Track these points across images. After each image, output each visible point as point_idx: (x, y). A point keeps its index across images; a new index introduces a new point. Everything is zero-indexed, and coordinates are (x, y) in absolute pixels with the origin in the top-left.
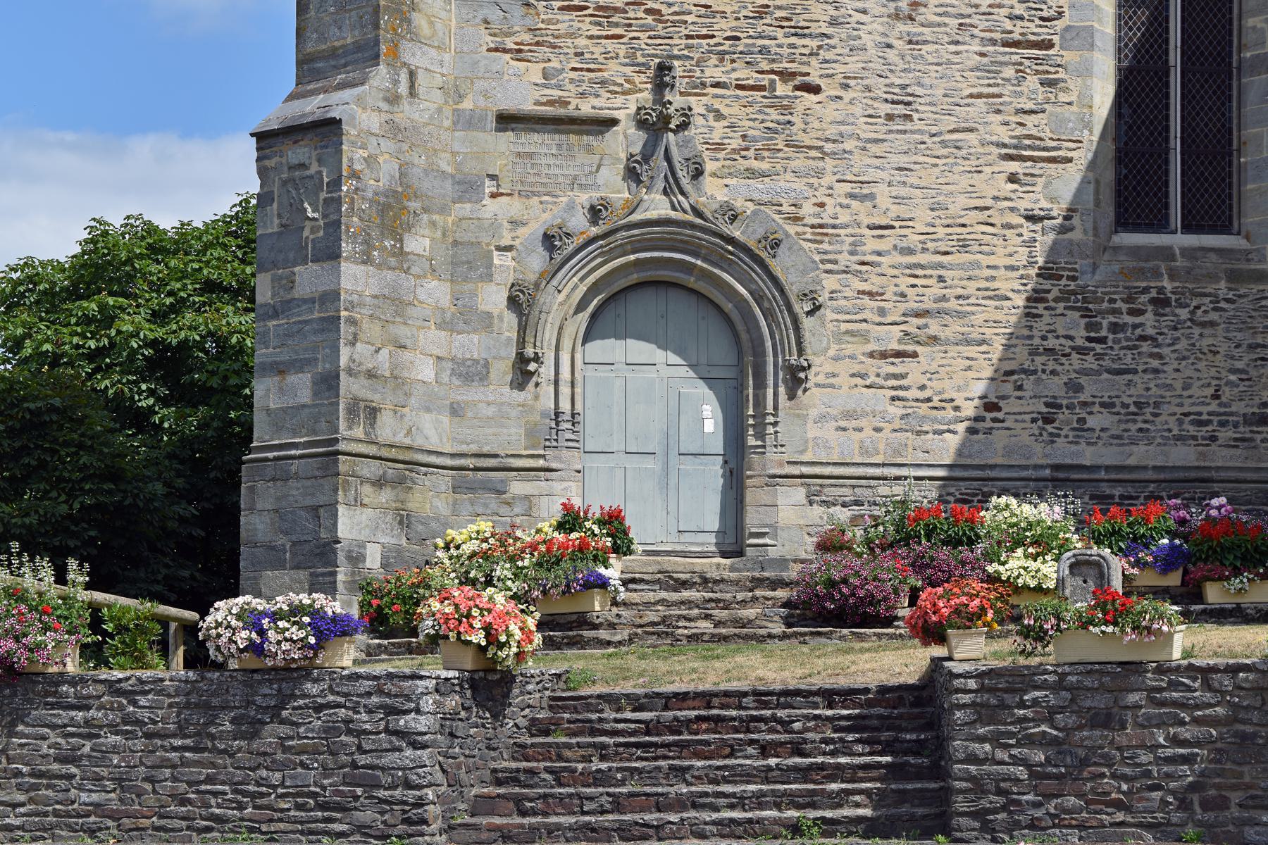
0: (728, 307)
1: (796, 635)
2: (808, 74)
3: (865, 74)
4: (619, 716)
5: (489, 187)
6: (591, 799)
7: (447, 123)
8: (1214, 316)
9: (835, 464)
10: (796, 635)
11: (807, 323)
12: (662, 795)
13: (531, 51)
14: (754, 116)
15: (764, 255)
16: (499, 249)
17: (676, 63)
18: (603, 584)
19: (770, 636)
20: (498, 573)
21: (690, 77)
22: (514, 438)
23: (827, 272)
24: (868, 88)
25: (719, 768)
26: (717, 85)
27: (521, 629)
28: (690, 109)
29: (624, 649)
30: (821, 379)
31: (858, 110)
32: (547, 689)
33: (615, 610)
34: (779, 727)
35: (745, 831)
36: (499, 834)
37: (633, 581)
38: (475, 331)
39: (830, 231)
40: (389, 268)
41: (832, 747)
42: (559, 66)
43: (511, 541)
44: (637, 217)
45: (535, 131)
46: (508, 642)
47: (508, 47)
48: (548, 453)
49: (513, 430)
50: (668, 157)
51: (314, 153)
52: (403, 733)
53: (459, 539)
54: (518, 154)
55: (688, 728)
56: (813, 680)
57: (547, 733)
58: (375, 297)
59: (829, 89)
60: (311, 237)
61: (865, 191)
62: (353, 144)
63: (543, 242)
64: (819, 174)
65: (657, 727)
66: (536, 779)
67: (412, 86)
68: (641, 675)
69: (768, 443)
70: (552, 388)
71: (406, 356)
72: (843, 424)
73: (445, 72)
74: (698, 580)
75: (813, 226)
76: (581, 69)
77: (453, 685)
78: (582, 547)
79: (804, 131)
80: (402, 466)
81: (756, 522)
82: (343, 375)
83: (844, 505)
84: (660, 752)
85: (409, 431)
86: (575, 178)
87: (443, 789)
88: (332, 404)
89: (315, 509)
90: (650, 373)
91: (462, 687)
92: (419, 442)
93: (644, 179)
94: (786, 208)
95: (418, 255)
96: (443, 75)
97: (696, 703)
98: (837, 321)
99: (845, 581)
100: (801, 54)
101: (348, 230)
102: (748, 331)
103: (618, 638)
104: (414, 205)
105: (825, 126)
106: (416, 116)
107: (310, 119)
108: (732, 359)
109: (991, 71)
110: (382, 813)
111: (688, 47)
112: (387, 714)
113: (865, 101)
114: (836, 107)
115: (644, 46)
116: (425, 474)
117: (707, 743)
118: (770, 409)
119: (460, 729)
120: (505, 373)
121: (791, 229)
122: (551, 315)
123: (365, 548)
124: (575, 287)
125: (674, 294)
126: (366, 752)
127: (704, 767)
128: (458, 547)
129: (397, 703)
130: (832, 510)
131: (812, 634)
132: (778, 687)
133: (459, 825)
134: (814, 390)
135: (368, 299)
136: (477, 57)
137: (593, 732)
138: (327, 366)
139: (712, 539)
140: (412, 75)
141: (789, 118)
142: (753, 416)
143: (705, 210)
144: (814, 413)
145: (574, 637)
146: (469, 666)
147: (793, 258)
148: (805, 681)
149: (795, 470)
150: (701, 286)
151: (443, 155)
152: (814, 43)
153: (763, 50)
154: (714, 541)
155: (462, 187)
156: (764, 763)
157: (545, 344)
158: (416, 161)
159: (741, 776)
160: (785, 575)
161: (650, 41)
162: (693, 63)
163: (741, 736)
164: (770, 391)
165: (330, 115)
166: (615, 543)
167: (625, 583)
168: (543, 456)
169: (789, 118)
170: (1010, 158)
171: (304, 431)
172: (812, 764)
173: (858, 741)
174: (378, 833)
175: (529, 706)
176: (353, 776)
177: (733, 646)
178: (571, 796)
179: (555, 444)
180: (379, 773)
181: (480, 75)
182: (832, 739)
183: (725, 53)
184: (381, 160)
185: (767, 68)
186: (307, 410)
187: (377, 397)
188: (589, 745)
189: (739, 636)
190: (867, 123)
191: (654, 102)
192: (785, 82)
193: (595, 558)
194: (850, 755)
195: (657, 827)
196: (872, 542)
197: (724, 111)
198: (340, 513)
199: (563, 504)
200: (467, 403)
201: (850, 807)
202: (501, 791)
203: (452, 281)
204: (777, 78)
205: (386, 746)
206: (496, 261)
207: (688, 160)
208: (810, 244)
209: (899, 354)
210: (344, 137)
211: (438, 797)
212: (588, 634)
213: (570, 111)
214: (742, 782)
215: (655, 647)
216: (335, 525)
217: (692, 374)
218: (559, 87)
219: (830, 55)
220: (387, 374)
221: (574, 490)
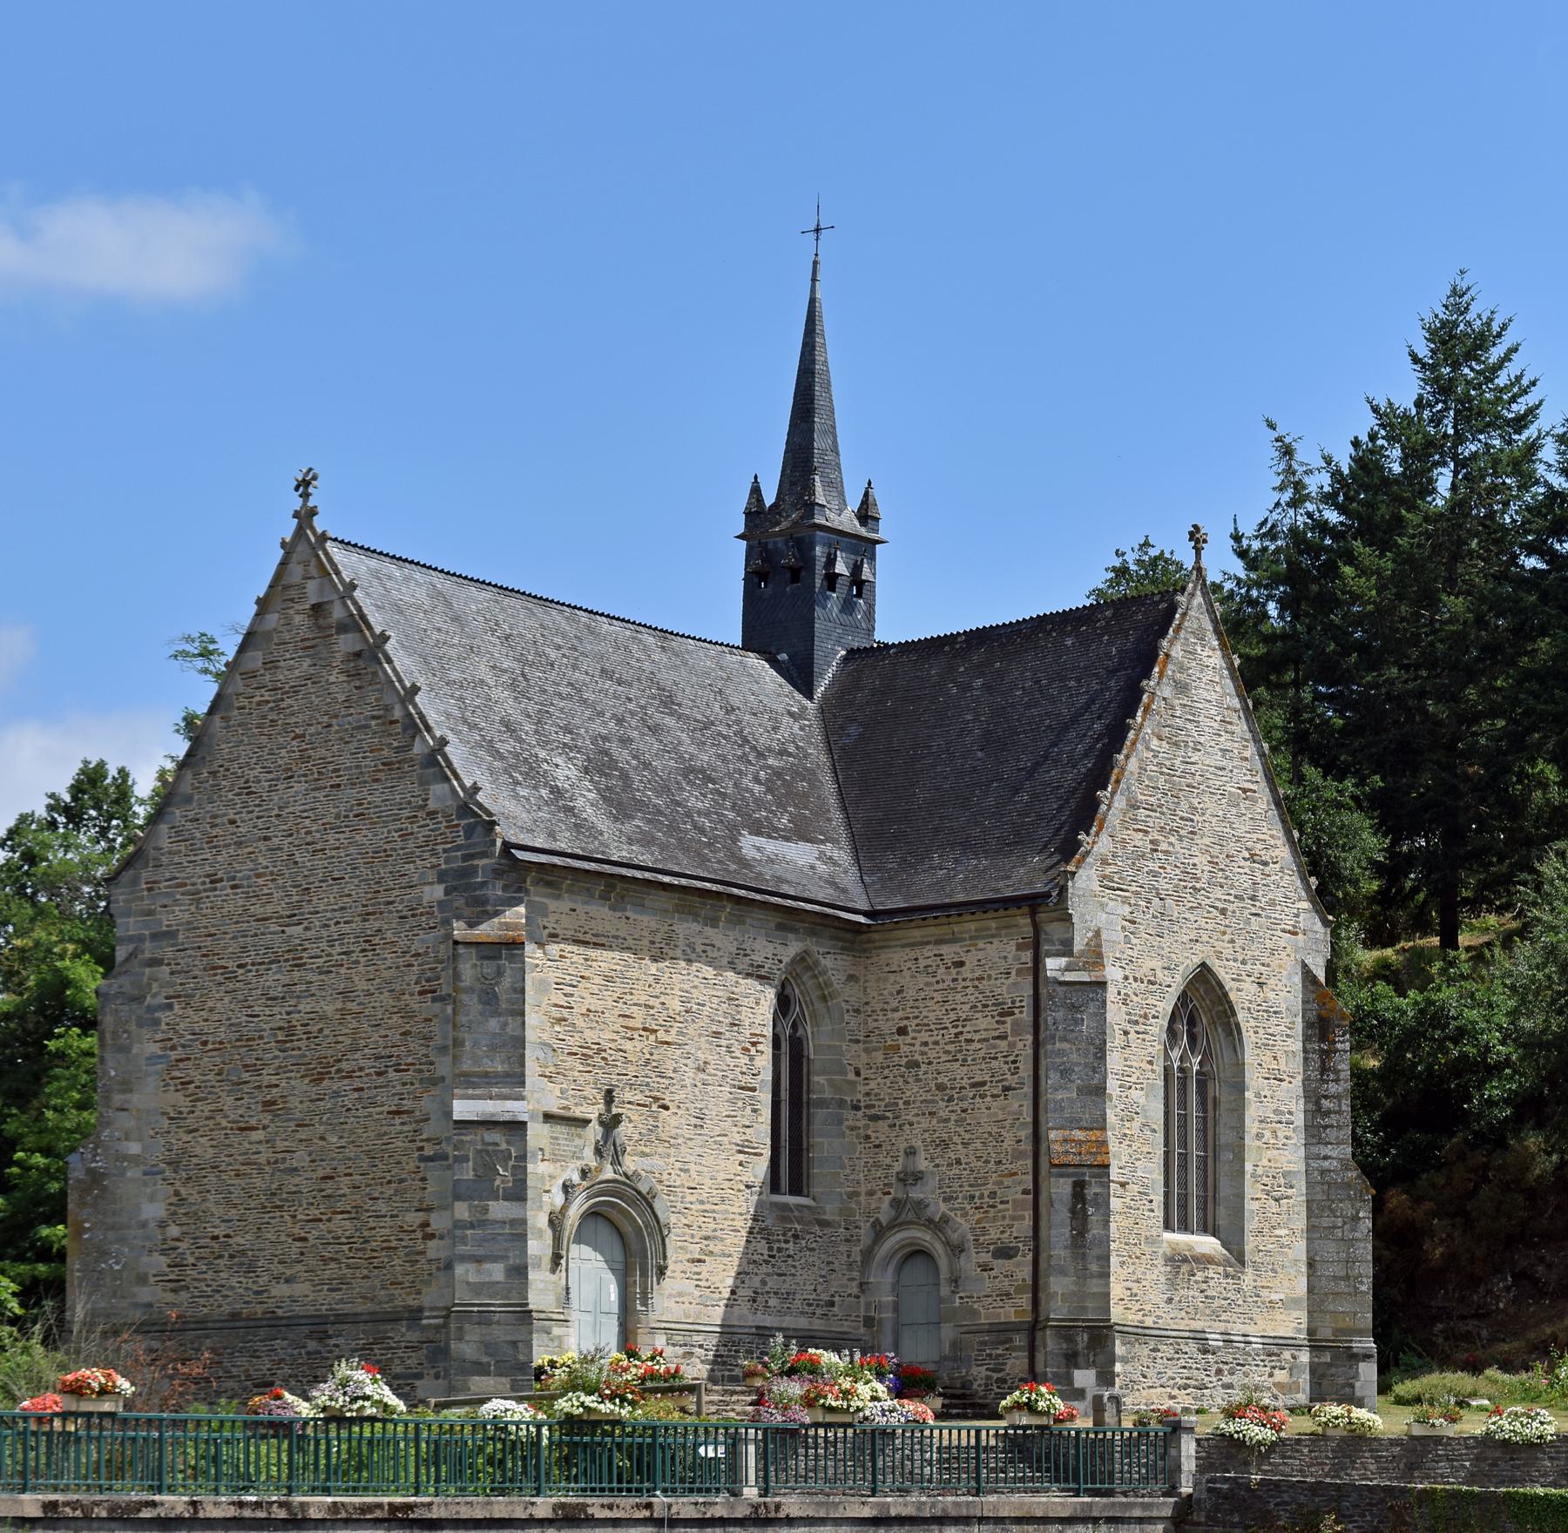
8: (814, 1245)
26: (629, 1103)
59: (673, 1110)
89: (514, 1344)
109: (732, 1102)
121: (659, 1187)
152: (667, 1082)
153: (647, 1085)
170: (740, 1152)
209: (699, 1261)
213: (570, 1114)
218: (567, 1099)
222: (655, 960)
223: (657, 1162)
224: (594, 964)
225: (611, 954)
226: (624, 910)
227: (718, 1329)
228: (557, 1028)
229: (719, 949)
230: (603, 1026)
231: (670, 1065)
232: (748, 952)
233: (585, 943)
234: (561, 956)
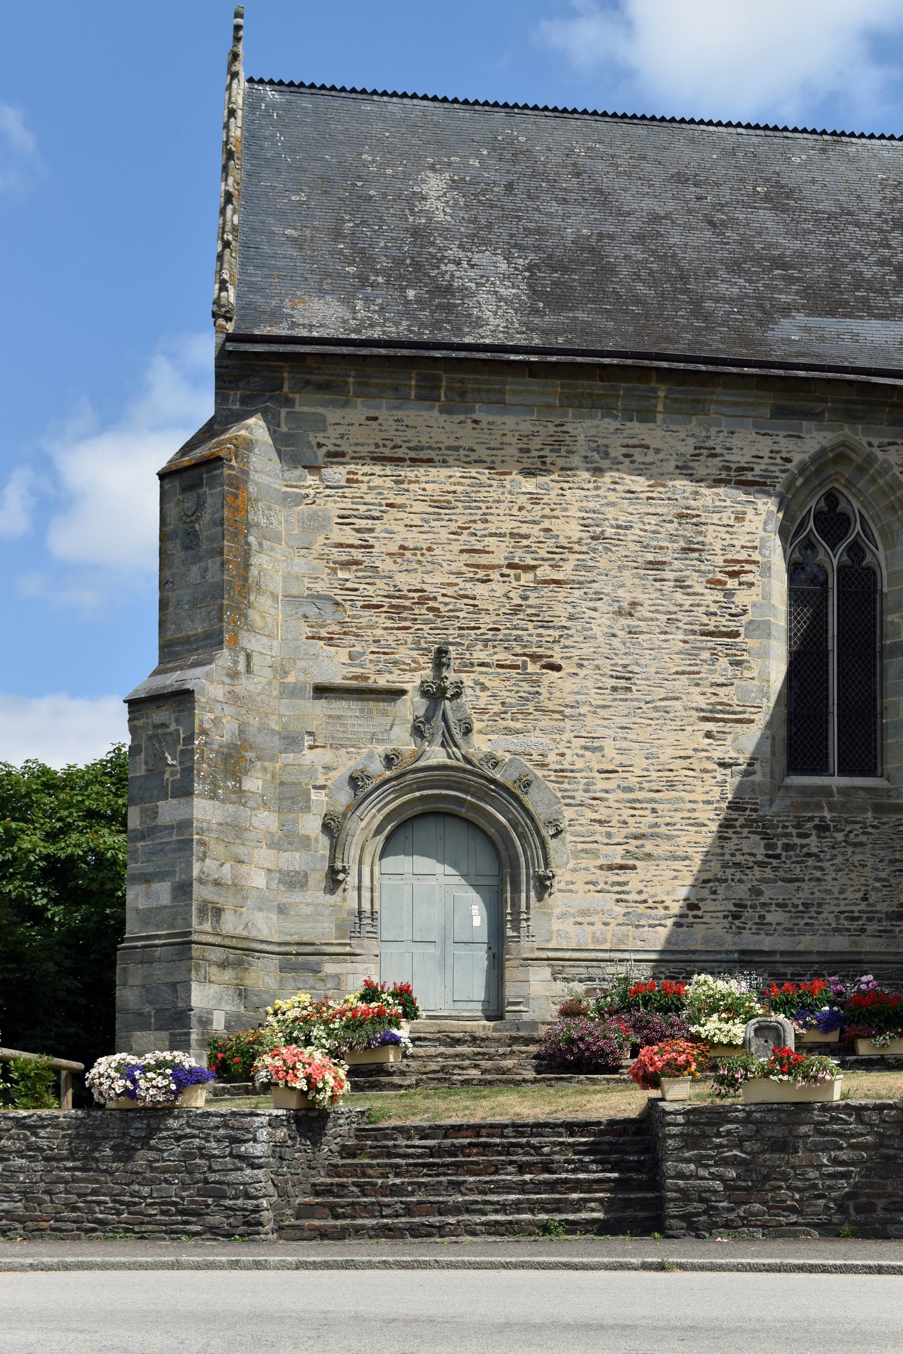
0: (492, 831)
1: (544, 1080)
3: (596, 656)
4: (409, 1143)
5: (308, 741)
6: (388, 1206)
7: (275, 693)
8: (863, 838)
9: (573, 950)
10: (544, 1080)
11: (552, 844)
12: (443, 1202)
15: (518, 792)
16: (315, 787)
17: (451, 648)
18: (396, 1041)
19: (525, 1081)
20: (315, 1033)
23: (566, 805)
24: (598, 667)
25: (486, 1182)
26: (482, 665)
27: (334, 1078)
28: (462, 683)
30: (562, 886)
31: (590, 683)
33: (405, 1061)
34: (532, 1151)
35: (507, 1230)
37: (419, 1039)
38: (297, 850)
39: (570, 774)
40: (231, 803)
42: (361, 650)
44: (421, 763)
45: (343, 699)
46: (324, 1088)
48: (353, 941)
49: (326, 925)
50: (445, 719)
51: (173, 716)
54: (330, 717)
55: (462, 1152)
56: (558, 1115)
57: (354, 1156)
58: (220, 824)
61: (596, 745)
62: (203, 708)
64: (561, 731)
66: (346, 1191)
67: (248, 665)
68: (426, 1111)
70: (356, 893)
71: (244, 868)
72: (579, 920)
75: (556, 771)
76: (378, 653)
78: (380, 1014)
79: (549, 699)
82: (195, 883)
83: (580, 981)
84: (441, 1170)
85: (247, 925)
86: (374, 734)
87: (275, 1199)
88: (186, 905)
89: (173, 985)
91: (289, 1122)
92: (254, 934)
93: (427, 735)
94: (535, 757)
97: (469, 1133)
101: (199, 774)
103: (407, 1082)
104: (250, 755)
105: (565, 695)
106: (251, 688)
107: (170, 690)
108: (494, 871)
109: (692, 653)
110: (228, 1217)
111: (460, 636)
112: (231, 1143)
117: (477, 1163)
118: (523, 909)
120: (320, 881)
121: (540, 773)
123: (212, 1014)
124: (374, 816)
126: (215, 1171)
127: (475, 1182)
128: (284, 1014)
129: (239, 1134)
130: (571, 984)
131: (556, 1079)
132: (531, 1120)
134: (557, 894)
137: (390, 1155)
138: (183, 876)
139: (479, 1006)
140: (248, 657)
141: (537, 689)
144: (557, 911)
149: (543, 955)
150: (471, 816)
151: (272, 717)
153: (518, 639)
155: (287, 741)
156: (522, 1178)
158: (252, 721)
160: (535, 1034)
163: (503, 1158)
166: (404, 1010)
167: (413, 1040)
168: (350, 945)
169: (537, 689)
170: (707, 719)
173: (593, 1162)
176: (205, 1189)
177: (496, 1089)
178: (373, 1203)
180: (225, 1187)
183: (488, 640)
184: (224, 721)
185: (520, 652)
186: (167, 910)
187: (221, 900)
188: (386, 1165)
189: (500, 1081)
191: (434, 678)
192: (534, 662)
193: (390, 1022)
199: (365, 981)
200: (290, 904)
203: (279, 812)
205: (230, 1166)
206: (313, 797)
209: (622, 867)
212: (385, 1079)
215: (436, 1089)
216: (189, 996)
217: (463, 882)
218: (362, 666)
219: (568, 642)
220: (229, 882)
221: (373, 969)
222: (529, 473)
223: (536, 740)
224: (413, 487)
225: (444, 472)
226: (473, 411)
227: (654, 956)
228: (341, 575)
229: (657, 451)
230: (429, 567)
231: (562, 611)
232: (718, 450)
233: (397, 461)
234: (348, 481)
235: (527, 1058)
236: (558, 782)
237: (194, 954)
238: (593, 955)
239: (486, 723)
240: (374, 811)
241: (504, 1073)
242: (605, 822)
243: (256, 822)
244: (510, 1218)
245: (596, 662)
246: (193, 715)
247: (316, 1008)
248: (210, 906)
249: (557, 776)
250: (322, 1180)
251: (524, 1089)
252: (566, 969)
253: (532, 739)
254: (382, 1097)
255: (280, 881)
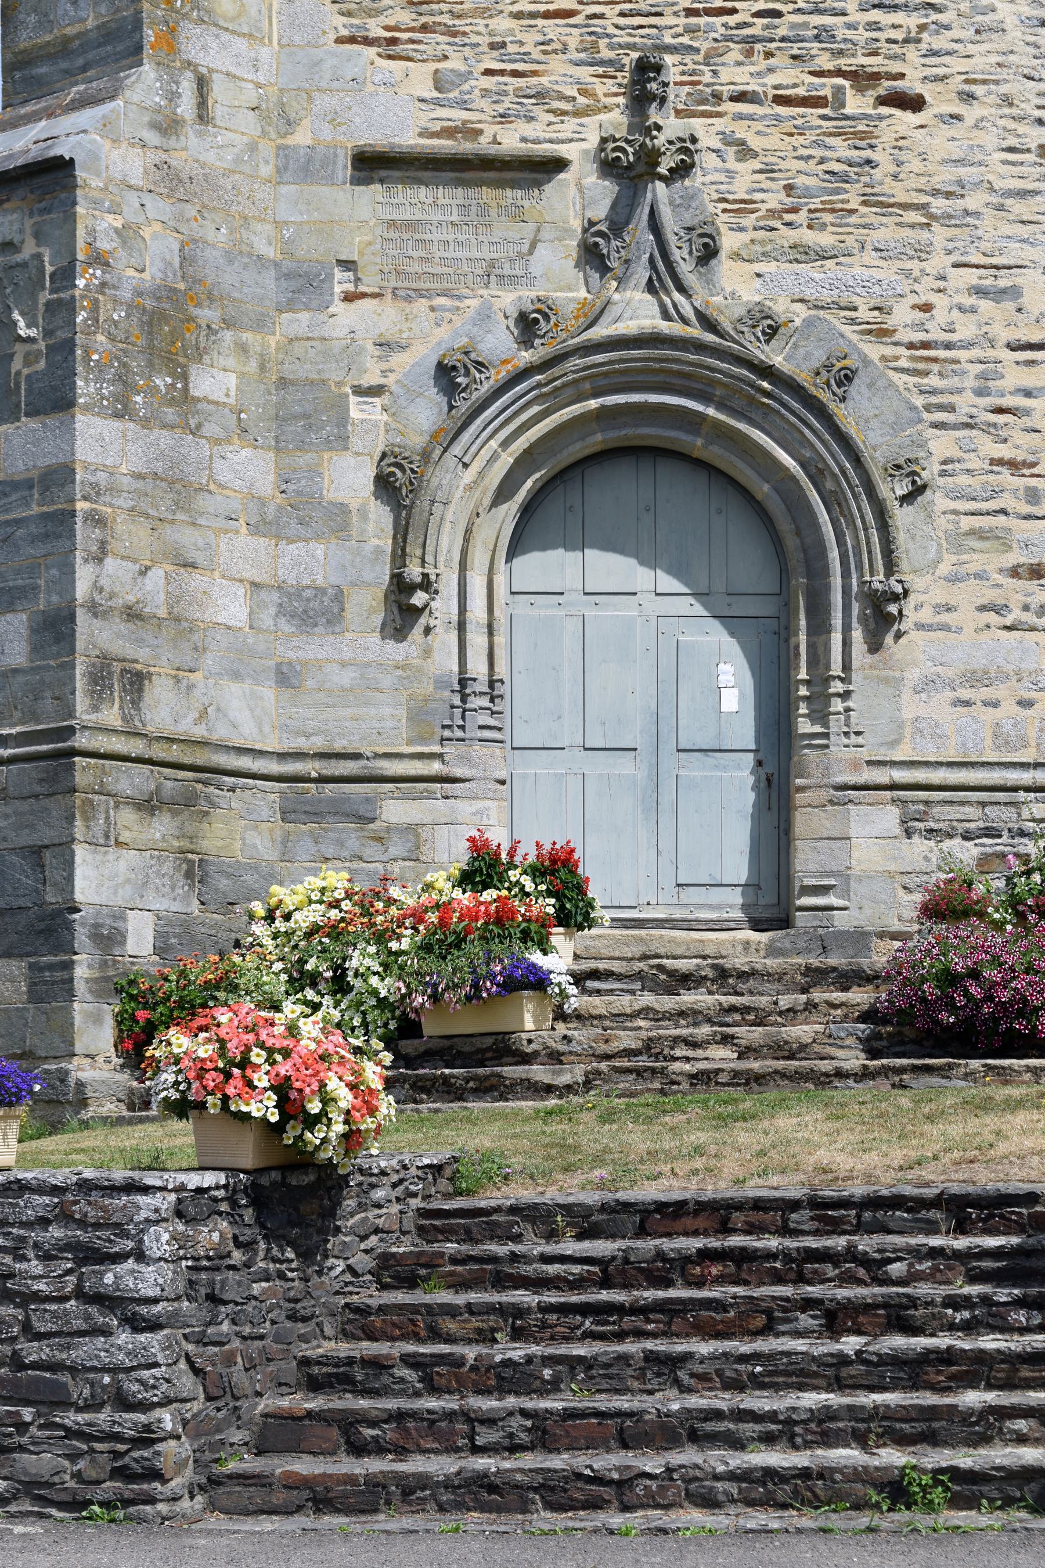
0: (763, 489)
1: (885, 1071)
2: (902, 76)
3: (1002, 74)
4: (551, 1249)
5: (341, 282)
6: (490, 1421)
7: (266, 170)
9: (951, 764)
10: (885, 1071)
11: (902, 517)
12: (630, 1414)
13: (412, 41)
14: (806, 152)
15: (825, 396)
16: (359, 391)
17: (669, 59)
18: (539, 981)
19: (840, 1074)
20: (354, 963)
21: (693, 83)
22: (389, 724)
23: (936, 426)
24: (1008, 101)
25: (744, 1359)
26: (740, 97)
27: (352, 1087)
28: (694, 140)
29: (575, 1099)
30: (926, 615)
31: (990, 139)
32: (414, 1195)
33: (561, 1028)
34: (861, 1272)
35: (796, 1492)
36: (306, 1494)
37: (595, 975)
38: (318, 537)
39: (942, 354)
40: (164, 426)
41: (966, 1314)
42: (462, 68)
43: (380, 905)
44: (600, 332)
45: (420, 182)
46: (323, 1113)
47: (372, 35)
48: (448, 749)
49: (387, 711)
50: (655, 226)
51: (29, 223)
52: (110, 1298)
53: (290, 903)
54: (392, 224)
55: (683, 1274)
56: (927, 1173)
57: (411, 1282)
58: (139, 476)
60: (26, 371)
61: (1003, 283)
62: (96, 203)
63: (437, 378)
64: (922, 252)
65: (623, 1272)
66: (386, 1379)
67: (202, 103)
68: (599, 1160)
69: (833, 729)
70: (454, 636)
71: (196, 581)
72: (965, 694)
73: (262, 80)
74: (710, 973)
75: (911, 346)
76: (502, 73)
77: (215, 1200)
78: (502, 917)
79: (895, 177)
80: (189, 775)
81: (812, 868)
82: (81, 615)
83: (967, 836)
84: (629, 1322)
85: (203, 714)
86: (492, 264)
87: (196, 1406)
88: (62, 666)
89: (35, 853)
90: (627, 608)
91: (234, 1203)
92: (221, 732)
93: (614, 264)
94: (863, 314)
95: (216, 403)
96: (259, 86)
97: (700, 1222)
98: (955, 512)
99: (974, 974)
100: (890, 41)
101: (87, 358)
102: (798, 533)
103: (565, 1079)
104: (207, 314)
105: (931, 168)
106: (210, 157)
107: (20, 162)
108: (769, 583)
110: (73, 1457)
111: (690, 30)
112: (80, 1262)
113: (1001, 122)
114: (952, 133)
115: (612, 30)
116: (232, 790)
117: (718, 1305)
118: (836, 669)
119: (231, 1284)
120: (372, 611)
121: (874, 351)
122: (452, 508)
123: (123, 918)
124: (494, 458)
125: (667, 472)
126: (40, 1336)
127: (713, 1357)
128: (287, 917)
129: (99, 1239)
130: (947, 844)
131: (915, 1069)
132: (858, 1190)
133: (230, 1477)
134: (914, 635)
135: (126, 480)
136: (319, 53)
137: (502, 1282)
138: (55, 598)
139: (736, 897)
140: (202, 84)
141: (868, 153)
142: (807, 683)
143: (721, 319)
144: (913, 675)
145: (487, 1077)
146: (248, 1161)
147: (876, 401)
148: (911, 1175)
149: (882, 776)
150: (717, 454)
151: (259, 227)
153: (823, 35)
154: (740, 901)
155: (294, 284)
156: (834, 1347)
157: (441, 559)
158: (211, 236)
159: (787, 1374)
160: (864, 962)
161: (622, 21)
162: (700, 58)
163: (785, 1291)
164: (836, 639)
165: (57, 151)
166: (561, 909)
167: (579, 979)
168: (440, 756)
169: (868, 153)
171: (17, 715)
172: (928, 1351)
173: (1019, 1303)
174: (66, 1497)
175: (377, 1231)
176: (16, 1384)
177: (771, 1095)
178: (450, 1415)
179: (459, 734)
180: (65, 1378)
181: (324, 85)
182: (967, 1298)
183: (755, 39)
184: (146, 233)
185: (829, 66)
186: (21, 679)
187: (143, 654)
188: (490, 1309)
189: (783, 1075)
190: (1005, 162)
191: (631, 128)
192: (860, 90)
193: (526, 936)
194: (1002, 1330)
195: (619, 1484)
196: (1022, 902)
197: (755, 143)
198: (78, 859)
199: (472, 840)
200: (305, 663)
201: (1006, 1442)
202: (315, 1403)
203: (277, 450)
204: (847, 84)
205: (78, 1324)
206: (354, 414)
207: (690, 229)
208: (905, 378)
210: (79, 192)
211: (185, 1423)
212: (511, 1072)
213: (483, 145)
214: (788, 1386)
215: (632, 1095)
216: (70, 879)
217: (699, 609)
218: (463, 105)
219: (940, 42)
220: (162, 613)
221: (494, 814)
235: (845, 1018)
236: (916, 373)
237: (80, 779)
238: (996, 777)
239: (751, 234)
240: (493, 444)
241: (791, 1057)
242: (1025, 464)
243: (223, 472)
244: (801, 1459)
245: (1003, 89)
246: (70, 218)
247: (360, 904)
248: (117, 667)
249: (913, 359)
250: (325, 1348)
251: (838, 1096)
252: (935, 810)
253: (857, 270)
254: (504, 1116)
255: (281, 611)
